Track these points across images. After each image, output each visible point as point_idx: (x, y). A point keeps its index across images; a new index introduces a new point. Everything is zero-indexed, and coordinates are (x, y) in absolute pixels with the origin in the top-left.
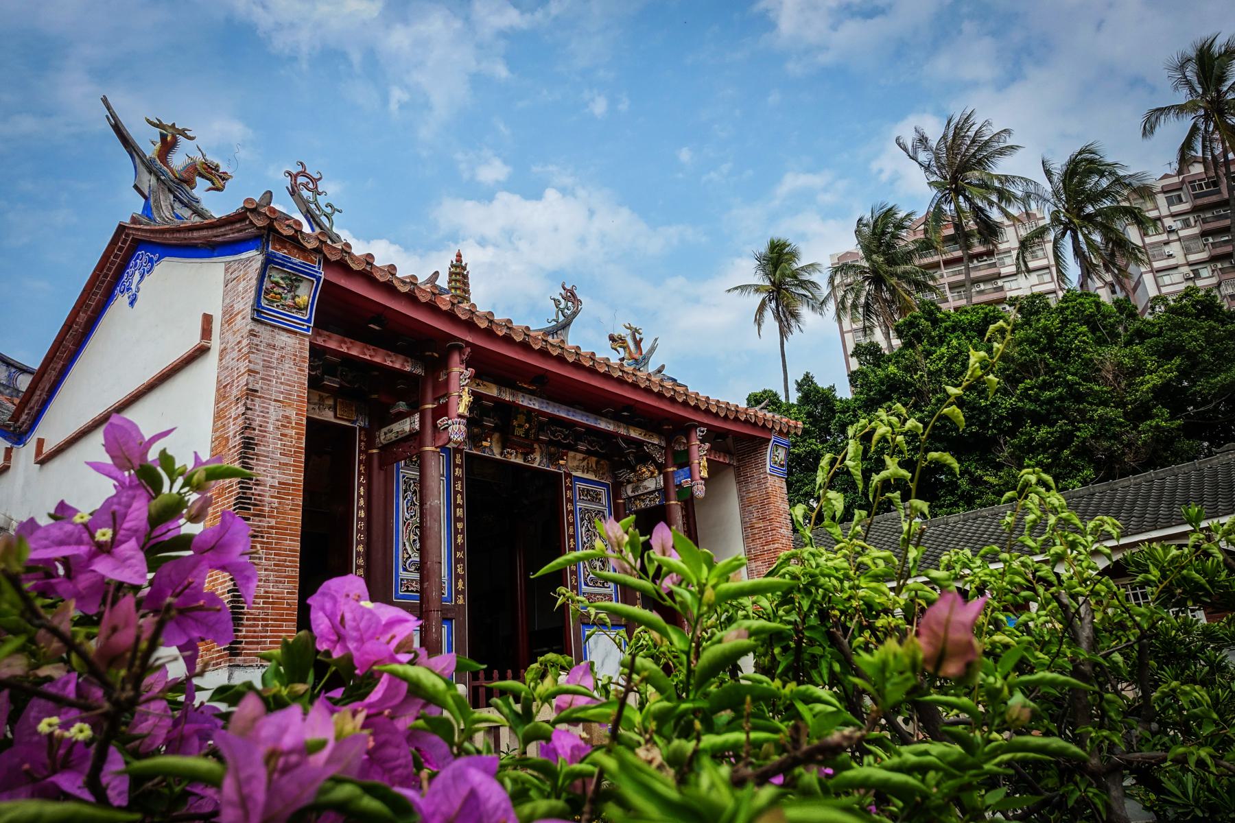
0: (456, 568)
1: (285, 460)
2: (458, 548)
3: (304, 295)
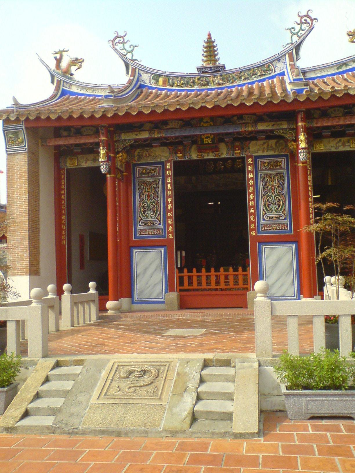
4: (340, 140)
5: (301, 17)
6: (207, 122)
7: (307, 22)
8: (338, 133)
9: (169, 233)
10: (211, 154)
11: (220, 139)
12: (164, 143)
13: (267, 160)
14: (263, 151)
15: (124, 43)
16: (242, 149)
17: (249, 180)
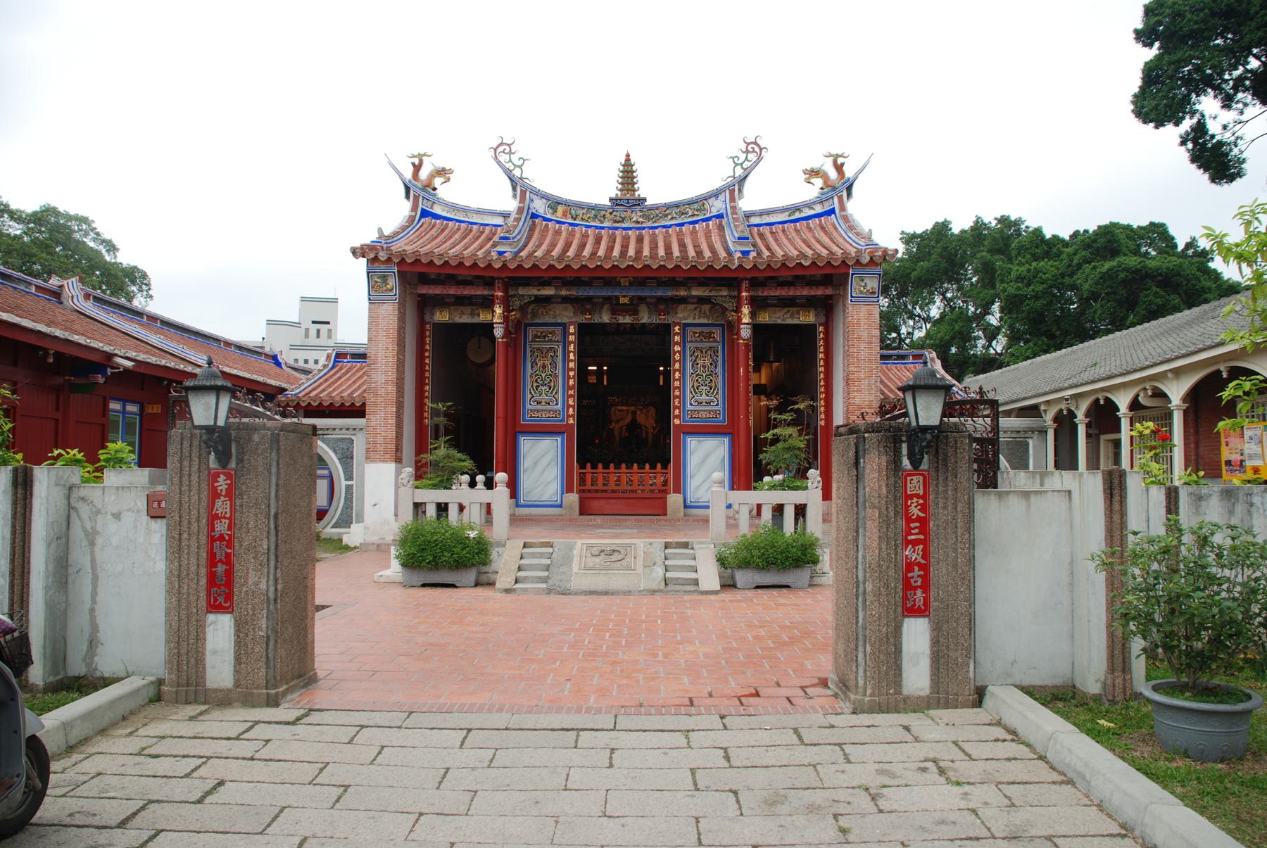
2: (570, 388)
3: (392, 282)
5: (748, 144)
7: (754, 151)
13: (698, 330)
15: (510, 153)
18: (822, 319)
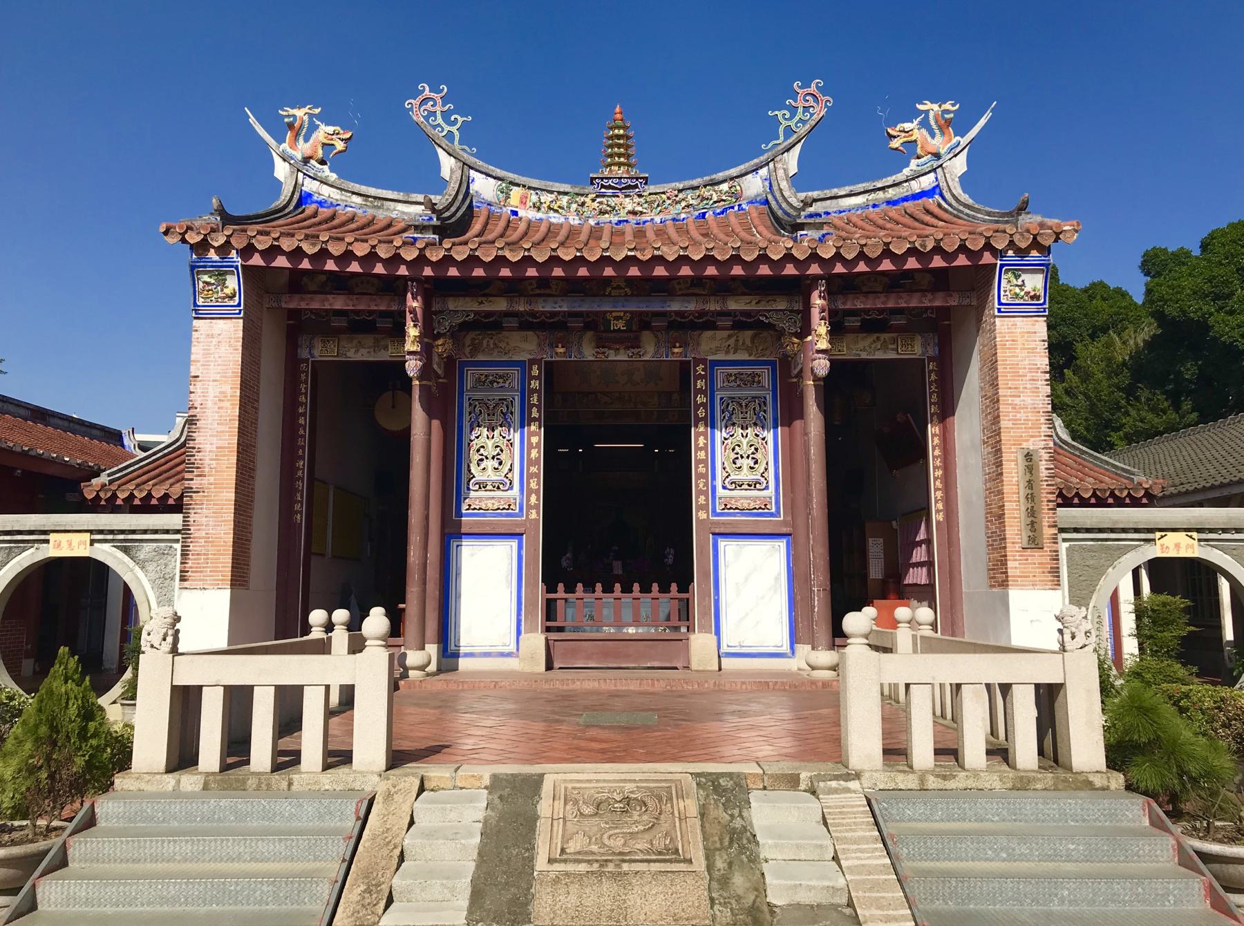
0: (529, 483)
1: (221, 428)
2: (532, 463)
3: (232, 283)
4: (878, 338)
6: (619, 287)
8: (874, 325)
9: (530, 507)
10: (622, 351)
11: (642, 322)
12: (529, 323)
13: (733, 370)
14: (727, 352)
16: (684, 345)
17: (697, 407)
18: (932, 351)
